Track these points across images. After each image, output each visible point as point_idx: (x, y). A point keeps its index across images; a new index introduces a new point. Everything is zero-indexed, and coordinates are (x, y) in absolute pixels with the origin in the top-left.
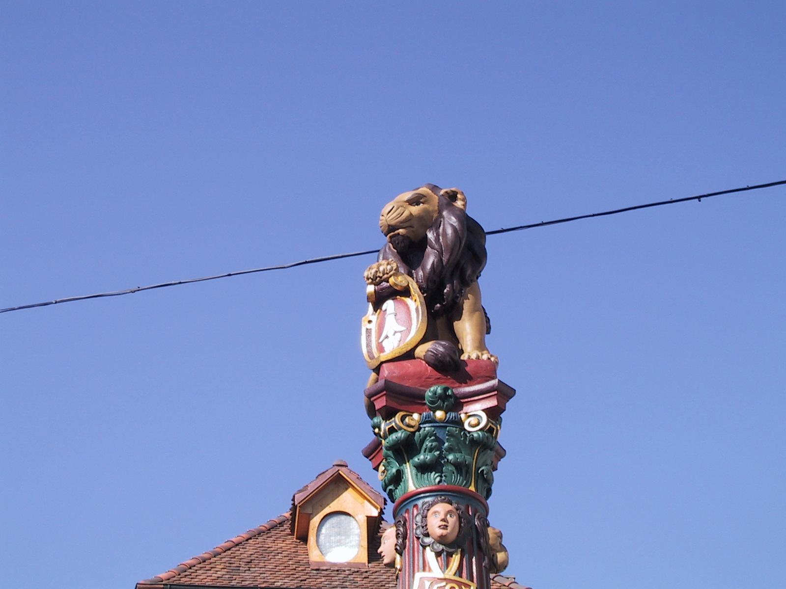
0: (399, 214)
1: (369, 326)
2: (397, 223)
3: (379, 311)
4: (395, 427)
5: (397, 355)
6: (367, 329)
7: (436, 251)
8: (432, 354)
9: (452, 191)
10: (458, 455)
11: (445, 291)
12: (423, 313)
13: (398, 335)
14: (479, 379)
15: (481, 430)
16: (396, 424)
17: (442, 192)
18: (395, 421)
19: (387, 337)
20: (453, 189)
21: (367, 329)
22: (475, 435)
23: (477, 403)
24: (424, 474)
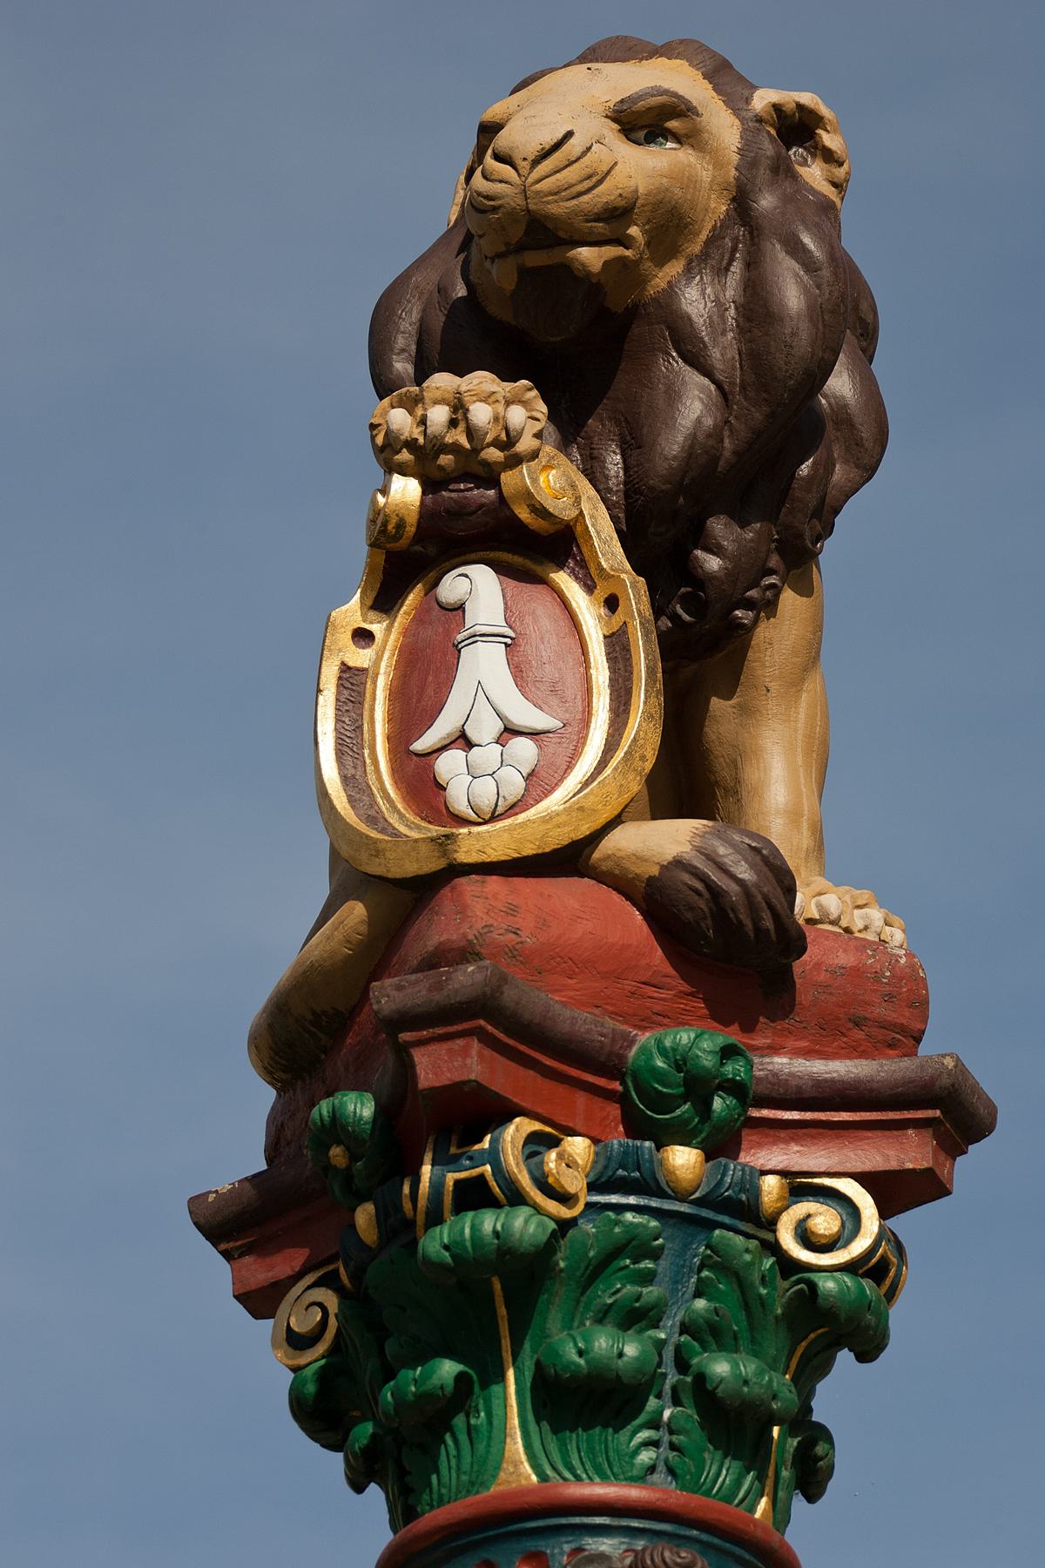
0: (589, 177)
1: (362, 658)
2: (575, 213)
3: (412, 599)
4: (493, 1184)
5: (529, 850)
6: (345, 668)
7: (713, 387)
8: (699, 886)
9: (800, 107)
10: (749, 1367)
11: (444, 493)
12: (651, 671)
13: (524, 750)
14: (859, 1035)
15: (850, 1267)
16: (498, 1170)
17: (763, 99)
18: (494, 1156)
19: (463, 740)
20: (806, 98)
21: (345, 668)
22: (828, 1285)
23: (793, 1139)
24: (616, 1431)
